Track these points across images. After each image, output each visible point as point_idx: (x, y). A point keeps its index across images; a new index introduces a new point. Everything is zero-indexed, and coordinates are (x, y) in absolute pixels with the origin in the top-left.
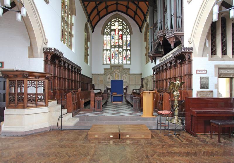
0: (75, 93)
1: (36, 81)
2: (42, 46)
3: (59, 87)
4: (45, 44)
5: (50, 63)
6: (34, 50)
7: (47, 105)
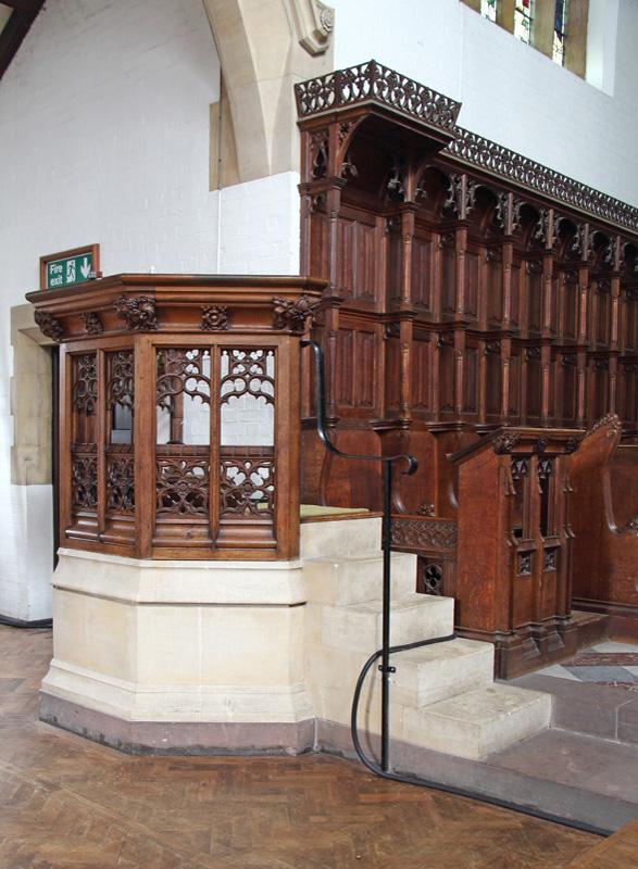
0: (543, 457)
1: (208, 347)
2: (287, 75)
3: (442, 407)
4: (315, 55)
5: (343, 200)
6: (238, 122)
7: (285, 548)
